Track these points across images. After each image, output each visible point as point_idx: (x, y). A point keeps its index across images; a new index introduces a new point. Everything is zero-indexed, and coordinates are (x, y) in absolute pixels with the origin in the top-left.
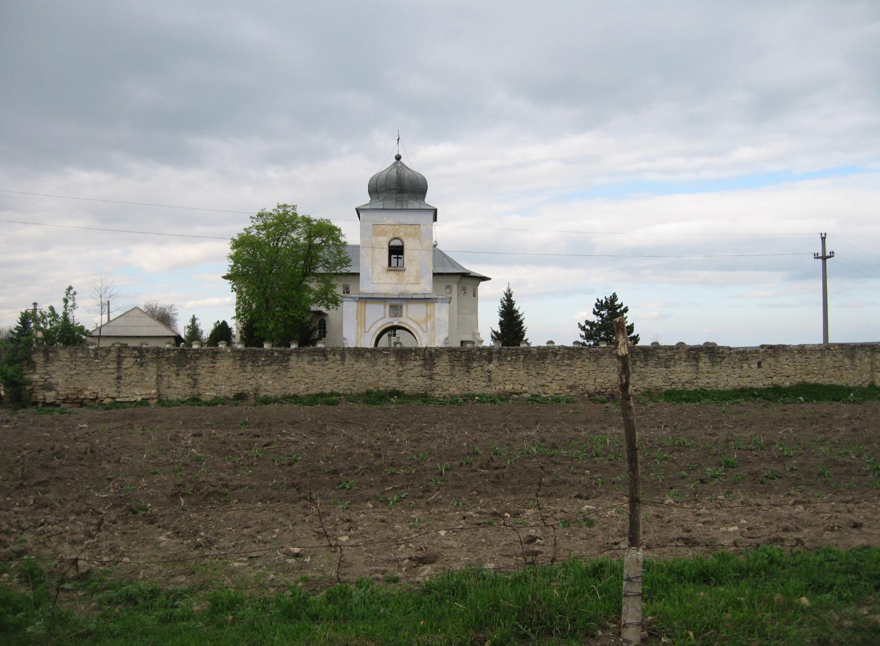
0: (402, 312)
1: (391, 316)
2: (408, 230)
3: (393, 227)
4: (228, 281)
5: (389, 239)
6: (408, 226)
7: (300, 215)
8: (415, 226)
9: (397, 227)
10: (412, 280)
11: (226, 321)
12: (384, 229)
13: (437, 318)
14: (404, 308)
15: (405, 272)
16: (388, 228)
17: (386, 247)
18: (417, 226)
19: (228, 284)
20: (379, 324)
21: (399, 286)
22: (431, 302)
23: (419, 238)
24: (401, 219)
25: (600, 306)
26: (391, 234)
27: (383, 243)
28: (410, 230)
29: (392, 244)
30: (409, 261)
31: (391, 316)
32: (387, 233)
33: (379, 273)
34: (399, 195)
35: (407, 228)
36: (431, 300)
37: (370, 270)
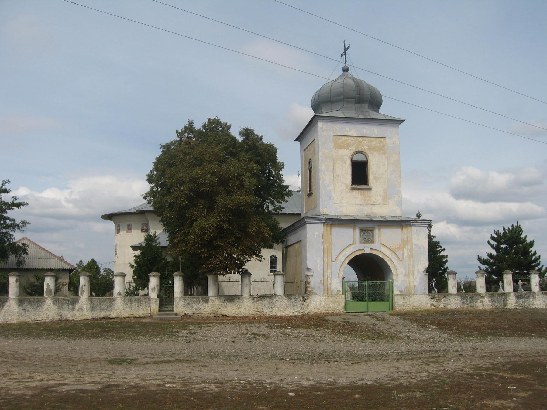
0: (373, 237)
1: (361, 242)
2: (373, 143)
3: (356, 139)
4: (121, 233)
5: (352, 152)
6: (373, 139)
7: (78, 263)
8: (380, 139)
9: (360, 139)
10: (379, 200)
11: (95, 259)
12: (346, 141)
13: (415, 245)
14: (376, 232)
15: (371, 191)
17: (349, 163)
18: (382, 139)
19: (260, 135)
20: (348, 251)
21: (365, 208)
22: (407, 226)
23: (384, 153)
25: (499, 239)
26: (354, 147)
27: (345, 157)
28: (374, 143)
29: (355, 158)
30: (375, 178)
31: (361, 242)
32: (349, 145)
34: (357, 105)
35: (372, 141)
36: (407, 223)
37: (332, 187)
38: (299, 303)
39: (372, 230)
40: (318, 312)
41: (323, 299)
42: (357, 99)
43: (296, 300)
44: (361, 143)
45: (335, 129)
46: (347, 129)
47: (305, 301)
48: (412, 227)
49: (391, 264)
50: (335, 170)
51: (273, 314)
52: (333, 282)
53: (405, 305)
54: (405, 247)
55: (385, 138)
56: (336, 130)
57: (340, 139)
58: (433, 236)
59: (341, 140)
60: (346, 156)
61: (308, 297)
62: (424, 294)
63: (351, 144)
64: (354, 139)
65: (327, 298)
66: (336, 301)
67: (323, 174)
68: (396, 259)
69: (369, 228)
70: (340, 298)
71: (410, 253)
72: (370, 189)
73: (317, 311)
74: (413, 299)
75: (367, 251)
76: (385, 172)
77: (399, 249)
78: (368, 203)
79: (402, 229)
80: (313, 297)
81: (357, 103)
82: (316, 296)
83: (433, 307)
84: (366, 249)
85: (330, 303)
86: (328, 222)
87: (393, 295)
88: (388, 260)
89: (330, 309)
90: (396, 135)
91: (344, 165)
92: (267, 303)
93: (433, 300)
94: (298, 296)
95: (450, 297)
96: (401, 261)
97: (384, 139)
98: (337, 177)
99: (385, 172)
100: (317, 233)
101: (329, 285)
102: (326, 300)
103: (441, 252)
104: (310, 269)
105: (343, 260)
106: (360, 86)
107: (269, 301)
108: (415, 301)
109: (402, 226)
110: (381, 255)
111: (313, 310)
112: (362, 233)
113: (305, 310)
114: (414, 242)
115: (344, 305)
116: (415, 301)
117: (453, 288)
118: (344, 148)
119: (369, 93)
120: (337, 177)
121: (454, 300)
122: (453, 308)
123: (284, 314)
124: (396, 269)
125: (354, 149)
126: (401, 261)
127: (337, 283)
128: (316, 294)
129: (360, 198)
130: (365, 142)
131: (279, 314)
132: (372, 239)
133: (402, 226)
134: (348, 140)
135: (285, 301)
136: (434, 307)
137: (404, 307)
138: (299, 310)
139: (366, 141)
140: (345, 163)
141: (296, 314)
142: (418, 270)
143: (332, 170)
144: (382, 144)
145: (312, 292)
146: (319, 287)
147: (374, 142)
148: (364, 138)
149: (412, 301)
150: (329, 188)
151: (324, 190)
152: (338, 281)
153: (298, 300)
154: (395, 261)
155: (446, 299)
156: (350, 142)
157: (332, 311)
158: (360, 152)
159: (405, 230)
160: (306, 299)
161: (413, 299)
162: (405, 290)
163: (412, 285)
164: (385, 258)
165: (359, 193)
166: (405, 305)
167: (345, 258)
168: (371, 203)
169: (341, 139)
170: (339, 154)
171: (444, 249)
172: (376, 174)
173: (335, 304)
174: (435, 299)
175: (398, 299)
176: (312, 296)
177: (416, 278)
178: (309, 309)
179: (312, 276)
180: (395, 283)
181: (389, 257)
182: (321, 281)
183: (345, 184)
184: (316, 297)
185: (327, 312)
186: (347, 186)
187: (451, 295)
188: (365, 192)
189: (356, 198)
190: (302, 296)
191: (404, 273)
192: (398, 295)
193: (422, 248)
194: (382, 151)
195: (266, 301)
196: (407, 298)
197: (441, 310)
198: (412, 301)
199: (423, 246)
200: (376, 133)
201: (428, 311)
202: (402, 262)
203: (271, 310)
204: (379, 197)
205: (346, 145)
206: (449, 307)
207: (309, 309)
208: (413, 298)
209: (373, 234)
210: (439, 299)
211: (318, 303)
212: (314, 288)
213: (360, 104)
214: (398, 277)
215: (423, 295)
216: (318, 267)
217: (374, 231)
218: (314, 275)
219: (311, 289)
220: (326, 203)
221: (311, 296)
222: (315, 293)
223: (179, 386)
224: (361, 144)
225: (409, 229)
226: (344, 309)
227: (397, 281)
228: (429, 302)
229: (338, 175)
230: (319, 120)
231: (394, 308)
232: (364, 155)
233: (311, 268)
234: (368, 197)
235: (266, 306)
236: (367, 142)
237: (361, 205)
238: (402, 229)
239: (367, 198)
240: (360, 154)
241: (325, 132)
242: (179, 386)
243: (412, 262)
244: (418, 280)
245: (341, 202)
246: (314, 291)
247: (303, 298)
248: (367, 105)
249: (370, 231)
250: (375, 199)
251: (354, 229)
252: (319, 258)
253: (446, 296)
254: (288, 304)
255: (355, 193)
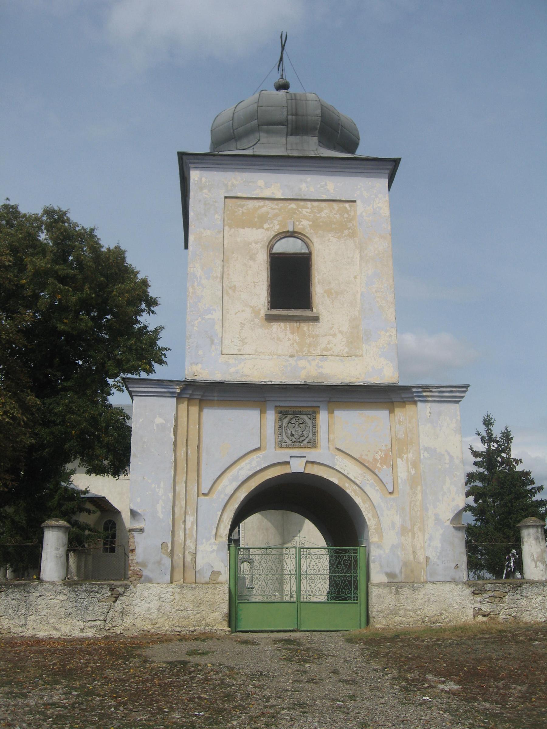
0: (315, 433)
1: (281, 444)
2: (323, 214)
3: (281, 204)
5: (272, 234)
6: (324, 204)
8: (341, 205)
9: (293, 205)
13: (426, 449)
14: (323, 416)
15: (318, 325)
16: (268, 207)
17: (262, 259)
18: (347, 205)
21: (302, 363)
22: (403, 403)
23: (353, 235)
24: (304, 186)
30: (329, 293)
33: (242, 325)
34: (292, 139)
35: (321, 210)
37: (217, 315)
38: (99, 604)
39: (313, 413)
40: (153, 630)
41: (168, 596)
42: (290, 126)
43: (93, 595)
44: (295, 213)
45: (230, 183)
46: (261, 183)
47: (117, 598)
48: (419, 404)
49: (364, 502)
50: (229, 274)
51: (28, 633)
52: (200, 548)
53: (401, 612)
54: (401, 458)
55: (355, 201)
56: (233, 185)
57: (242, 206)
58: (515, 459)
59: (245, 207)
60: (256, 243)
61: (126, 587)
62: (455, 582)
63: (270, 216)
64: (277, 205)
65: (178, 590)
66: (205, 599)
67: (196, 284)
68: (377, 488)
69: (304, 410)
70: (216, 591)
71: (413, 472)
72: (316, 319)
73: (149, 627)
74: (422, 596)
75: (297, 466)
76: (355, 277)
77: (384, 461)
78: (309, 352)
79: (392, 411)
80: (140, 589)
81: (291, 135)
82: (150, 585)
83: (480, 618)
84: (293, 461)
85: (187, 604)
86: (190, 392)
87: (370, 586)
88: (354, 491)
89: (185, 623)
90: (380, 196)
91: (251, 263)
92: (14, 602)
93: (479, 599)
94: (99, 585)
95: (527, 590)
96: (391, 493)
97: (351, 204)
98: (230, 292)
99: (355, 277)
100: (159, 420)
101: (189, 558)
102: (177, 596)
103: (534, 494)
104: (139, 514)
105: (230, 490)
106: (298, 98)
107: (18, 596)
108: (428, 601)
109: (392, 402)
110: (335, 479)
111: (139, 623)
112: (285, 421)
113: (114, 624)
114: (425, 441)
115: (226, 610)
116: (428, 601)
117: (536, 566)
118: (251, 224)
119: (319, 112)
120: (230, 292)
121: (540, 597)
122: (539, 620)
123: (56, 634)
124: (376, 515)
125: (277, 227)
126: (391, 493)
127: (212, 552)
128: (150, 581)
129: (289, 339)
130: (304, 211)
131: (41, 634)
132: (311, 436)
133: (392, 402)
134: (263, 207)
135: (62, 597)
136: (485, 619)
137: (397, 619)
138: (98, 623)
139: (308, 208)
140: (252, 258)
141: (90, 633)
142: (437, 516)
143: (219, 275)
144: (346, 215)
145: (139, 576)
146: (159, 563)
147: (326, 211)
148: (302, 203)
149: (420, 602)
150: (209, 316)
151: (196, 322)
152: (215, 547)
153: (98, 595)
154: (374, 493)
155: (519, 596)
156: (268, 213)
157: (192, 629)
158: (293, 234)
159: (400, 413)
160: (121, 595)
161: (422, 596)
162: (401, 572)
163: (422, 559)
164: (347, 485)
165: (286, 328)
166: (401, 612)
167: (235, 485)
168: (319, 352)
169: (244, 205)
170: (239, 240)
171: (541, 488)
172: (330, 283)
173: (202, 608)
174: (485, 595)
175: (379, 596)
176: (139, 585)
177: (430, 539)
178: (128, 621)
179: (141, 530)
180: (374, 553)
181: (358, 482)
182: (164, 544)
183: (251, 306)
184: (149, 589)
185: (178, 629)
186: (256, 312)
187: (532, 583)
188: (302, 325)
189: (278, 339)
190: (110, 585)
191: (398, 525)
192: (380, 585)
193: (447, 457)
194: (345, 231)
195: (11, 596)
196: (406, 592)
197: (499, 627)
198: (420, 602)
199: (449, 454)
200: (332, 191)
201: (464, 628)
202: (392, 496)
203: (23, 622)
204: (339, 336)
205: (256, 219)
206: (526, 618)
207: (128, 621)
208: (422, 592)
209: (314, 423)
210: (496, 594)
211: (155, 604)
212: (144, 565)
213: (298, 137)
214: (381, 537)
215: (453, 585)
216: (159, 508)
217: (317, 416)
218: (146, 530)
219: (137, 568)
220: (200, 353)
221: (135, 587)
222: (147, 576)
223: (527, 723)
224: (295, 216)
225: (410, 409)
226: (226, 624)
227: (379, 547)
228: (470, 605)
229: (235, 286)
230: (191, 165)
231: (371, 620)
232: (302, 240)
233: (139, 511)
234: (309, 337)
235: (10, 611)
236: (308, 210)
237: (292, 356)
238: (392, 411)
239: (308, 341)
240: (291, 239)
241: (205, 191)
242: (527, 723)
243: (419, 497)
244: (437, 543)
245: (240, 350)
246: (146, 572)
247: (112, 590)
248: (316, 138)
249: (305, 417)
250: (329, 343)
251: (263, 412)
252: (162, 485)
253: (517, 587)
254: (70, 605)
255: (277, 328)
